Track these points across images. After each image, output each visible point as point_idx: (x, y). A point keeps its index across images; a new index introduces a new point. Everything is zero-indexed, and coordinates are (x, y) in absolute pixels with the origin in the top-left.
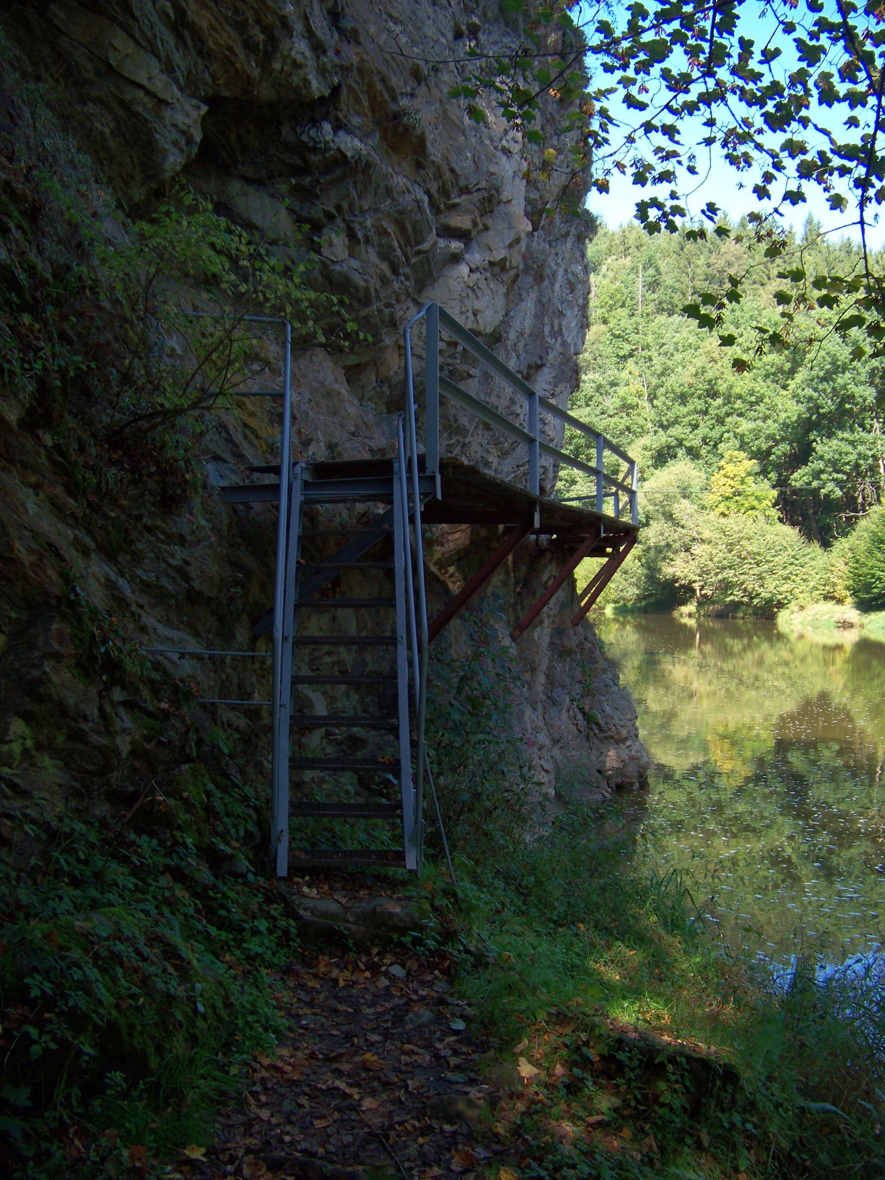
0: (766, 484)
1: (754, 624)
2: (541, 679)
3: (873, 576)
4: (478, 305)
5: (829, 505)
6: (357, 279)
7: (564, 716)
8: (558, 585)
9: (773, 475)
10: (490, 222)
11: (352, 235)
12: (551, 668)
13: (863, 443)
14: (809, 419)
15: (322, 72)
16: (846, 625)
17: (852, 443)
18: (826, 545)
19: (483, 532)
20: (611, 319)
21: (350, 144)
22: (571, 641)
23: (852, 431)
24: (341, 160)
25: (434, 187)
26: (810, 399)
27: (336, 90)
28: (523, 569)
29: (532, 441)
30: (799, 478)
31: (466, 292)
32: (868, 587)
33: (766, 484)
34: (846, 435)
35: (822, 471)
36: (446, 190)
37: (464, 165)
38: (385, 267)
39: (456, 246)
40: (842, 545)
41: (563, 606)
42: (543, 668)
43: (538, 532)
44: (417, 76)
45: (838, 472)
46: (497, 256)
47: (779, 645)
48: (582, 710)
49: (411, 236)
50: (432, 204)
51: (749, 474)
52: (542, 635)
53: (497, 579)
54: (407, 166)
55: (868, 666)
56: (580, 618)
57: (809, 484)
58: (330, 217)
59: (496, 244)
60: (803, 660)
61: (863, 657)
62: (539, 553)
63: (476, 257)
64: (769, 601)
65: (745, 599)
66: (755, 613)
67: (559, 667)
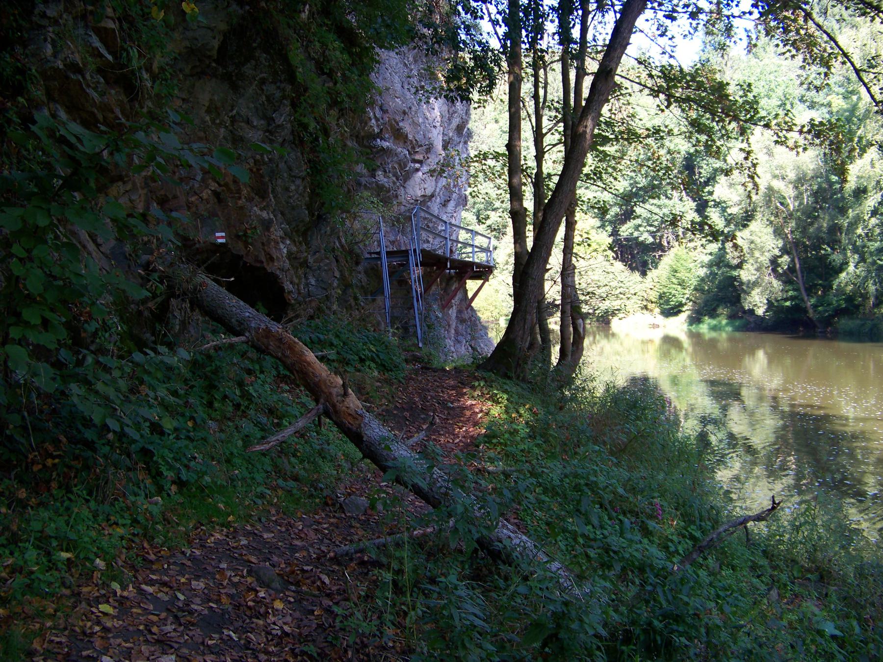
0: (605, 234)
1: (598, 327)
2: (453, 331)
3: (670, 293)
4: (426, 186)
5: (646, 248)
6: (386, 185)
7: (463, 348)
8: (457, 290)
9: (609, 229)
10: (429, 156)
11: (385, 171)
12: (457, 327)
13: (666, 206)
14: (631, 191)
15: (378, 126)
16: (655, 326)
17: (659, 207)
18: (644, 274)
19: (428, 270)
20: (500, 120)
21: (385, 144)
22: (466, 316)
23: (659, 199)
24: (383, 149)
25: (409, 148)
26: (632, 178)
27: (381, 130)
28: (444, 284)
29: (446, 222)
30: (626, 230)
31: (420, 184)
32: (667, 302)
33: (605, 234)
34: (656, 201)
35: (640, 226)
36: (413, 147)
37: (419, 137)
38: (394, 179)
39: (417, 165)
40: (652, 274)
41: (461, 300)
42: (454, 326)
43: (449, 269)
44: (404, 113)
45: (651, 226)
46: (432, 168)
47: (613, 340)
48: (471, 346)
49: (402, 165)
50: (410, 153)
51: (593, 228)
52: (453, 312)
53: (434, 288)
54: (401, 144)
55: (669, 352)
56: (469, 306)
57: (632, 234)
58: (379, 167)
59: (433, 162)
60: (629, 351)
61: (665, 347)
62: (450, 278)
63: (425, 168)
64: (607, 312)
65: (591, 311)
66: (598, 320)
67: (460, 327)
